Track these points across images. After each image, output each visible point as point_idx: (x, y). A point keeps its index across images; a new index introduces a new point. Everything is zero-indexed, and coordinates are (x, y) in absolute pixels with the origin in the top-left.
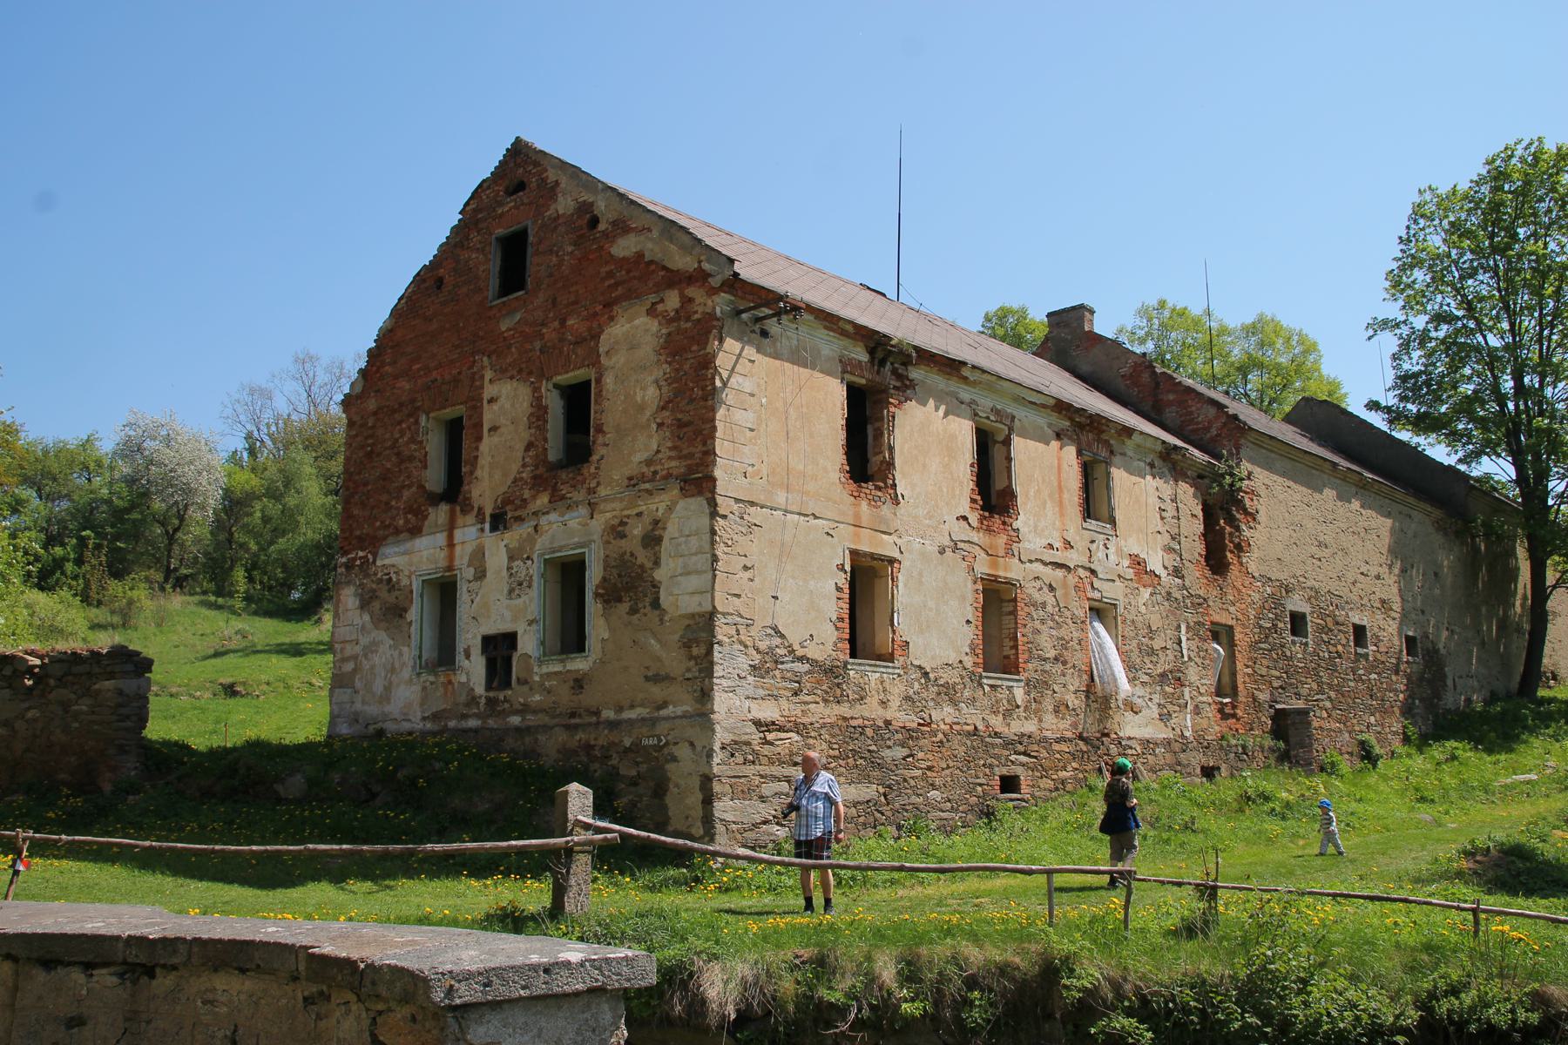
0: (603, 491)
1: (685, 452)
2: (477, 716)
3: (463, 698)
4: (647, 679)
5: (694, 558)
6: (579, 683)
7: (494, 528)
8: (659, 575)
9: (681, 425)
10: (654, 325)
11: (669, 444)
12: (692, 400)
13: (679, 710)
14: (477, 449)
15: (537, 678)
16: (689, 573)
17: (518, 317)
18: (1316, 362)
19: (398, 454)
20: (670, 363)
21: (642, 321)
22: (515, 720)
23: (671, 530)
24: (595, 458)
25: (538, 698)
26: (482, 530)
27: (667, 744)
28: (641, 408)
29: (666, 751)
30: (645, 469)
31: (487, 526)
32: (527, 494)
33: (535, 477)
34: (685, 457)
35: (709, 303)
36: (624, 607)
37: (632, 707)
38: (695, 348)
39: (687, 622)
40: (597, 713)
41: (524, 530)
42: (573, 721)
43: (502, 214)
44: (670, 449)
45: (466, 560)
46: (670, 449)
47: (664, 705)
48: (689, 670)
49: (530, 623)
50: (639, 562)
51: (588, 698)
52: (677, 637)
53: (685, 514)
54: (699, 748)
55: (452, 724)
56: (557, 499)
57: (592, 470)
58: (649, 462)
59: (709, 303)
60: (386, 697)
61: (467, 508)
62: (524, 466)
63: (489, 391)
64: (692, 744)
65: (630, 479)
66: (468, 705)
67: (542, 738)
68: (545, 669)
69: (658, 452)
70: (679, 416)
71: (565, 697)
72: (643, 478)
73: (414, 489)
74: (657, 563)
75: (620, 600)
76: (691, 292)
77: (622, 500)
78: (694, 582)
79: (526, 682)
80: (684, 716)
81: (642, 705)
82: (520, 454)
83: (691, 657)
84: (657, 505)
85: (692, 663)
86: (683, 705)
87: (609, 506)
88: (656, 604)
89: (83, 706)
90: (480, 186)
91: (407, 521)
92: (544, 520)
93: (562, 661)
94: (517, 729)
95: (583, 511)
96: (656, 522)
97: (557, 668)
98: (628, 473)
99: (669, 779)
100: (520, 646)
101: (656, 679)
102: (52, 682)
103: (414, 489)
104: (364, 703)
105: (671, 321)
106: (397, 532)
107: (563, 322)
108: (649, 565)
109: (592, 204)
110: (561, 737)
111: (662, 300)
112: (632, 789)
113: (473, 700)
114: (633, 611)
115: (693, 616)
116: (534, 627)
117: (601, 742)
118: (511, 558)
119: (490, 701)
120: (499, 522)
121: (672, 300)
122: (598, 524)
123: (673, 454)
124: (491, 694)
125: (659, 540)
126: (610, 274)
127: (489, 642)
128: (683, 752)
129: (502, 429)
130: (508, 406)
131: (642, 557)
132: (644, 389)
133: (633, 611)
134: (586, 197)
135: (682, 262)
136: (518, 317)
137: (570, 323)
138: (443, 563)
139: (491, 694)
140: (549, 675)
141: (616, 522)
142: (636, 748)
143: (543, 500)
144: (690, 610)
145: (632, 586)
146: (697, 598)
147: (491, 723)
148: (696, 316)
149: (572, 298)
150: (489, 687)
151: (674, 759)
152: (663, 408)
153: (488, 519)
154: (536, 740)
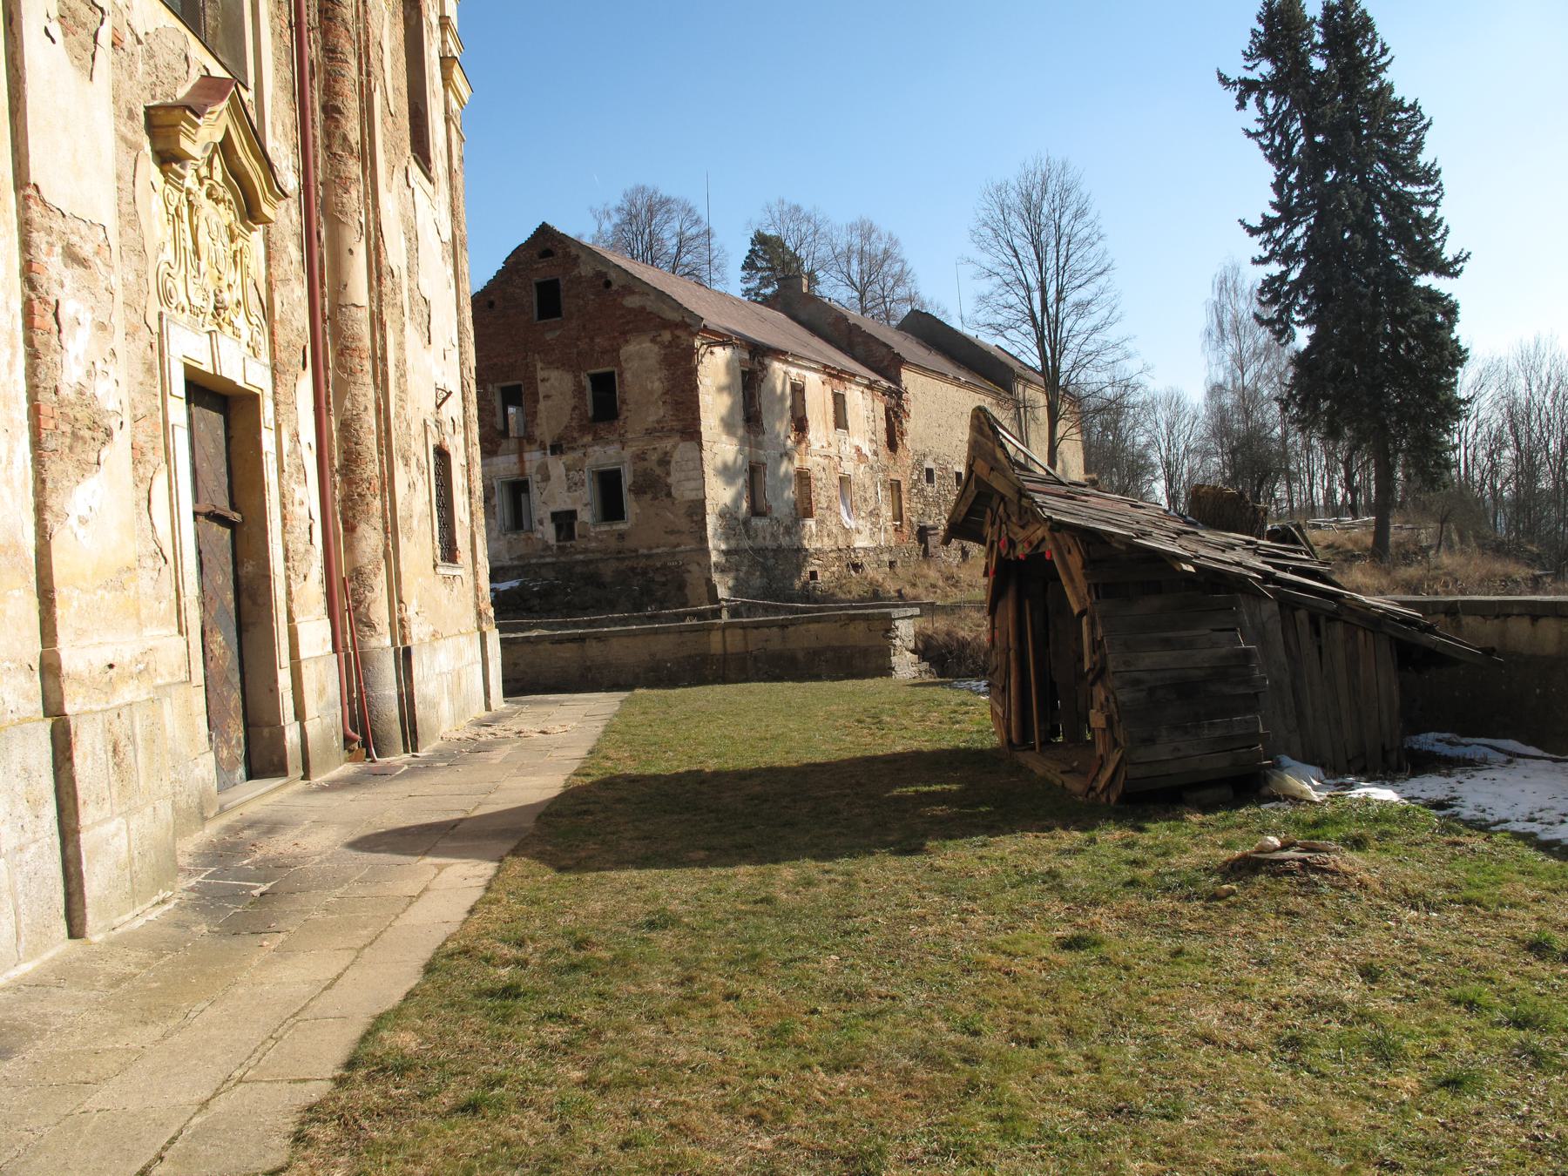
0: (629, 436)
6: (622, 536)
7: (553, 453)
8: (669, 480)
9: (677, 403)
10: (656, 348)
22: (581, 557)
23: (676, 456)
28: (651, 393)
32: (576, 435)
36: (649, 496)
41: (578, 454)
47: (678, 545)
51: (629, 543)
53: (682, 451)
56: (597, 439)
58: (658, 422)
63: (540, 374)
71: (613, 544)
72: (655, 430)
74: (668, 474)
76: (678, 332)
78: (692, 484)
84: (667, 444)
88: (669, 495)
92: (590, 450)
95: (617, 446)
96: (666, 453)
97: (606, 528)
101: (672, 532)
107: (592, 339)
113: (547, 547)
114: (655, 498)
118: (568, 470)
120: (556, 449)
121: (667, 336)
122: (627, 453)
126: (622, 316)
127: (555, 516)
128: (694, 568)
131: (658, 471)
133: (655, 498)
134: (600, 268)
142: (664, 566)
143: (588, 439)
145: (653, 485)
147: (562, 559)
150: (558, 540)
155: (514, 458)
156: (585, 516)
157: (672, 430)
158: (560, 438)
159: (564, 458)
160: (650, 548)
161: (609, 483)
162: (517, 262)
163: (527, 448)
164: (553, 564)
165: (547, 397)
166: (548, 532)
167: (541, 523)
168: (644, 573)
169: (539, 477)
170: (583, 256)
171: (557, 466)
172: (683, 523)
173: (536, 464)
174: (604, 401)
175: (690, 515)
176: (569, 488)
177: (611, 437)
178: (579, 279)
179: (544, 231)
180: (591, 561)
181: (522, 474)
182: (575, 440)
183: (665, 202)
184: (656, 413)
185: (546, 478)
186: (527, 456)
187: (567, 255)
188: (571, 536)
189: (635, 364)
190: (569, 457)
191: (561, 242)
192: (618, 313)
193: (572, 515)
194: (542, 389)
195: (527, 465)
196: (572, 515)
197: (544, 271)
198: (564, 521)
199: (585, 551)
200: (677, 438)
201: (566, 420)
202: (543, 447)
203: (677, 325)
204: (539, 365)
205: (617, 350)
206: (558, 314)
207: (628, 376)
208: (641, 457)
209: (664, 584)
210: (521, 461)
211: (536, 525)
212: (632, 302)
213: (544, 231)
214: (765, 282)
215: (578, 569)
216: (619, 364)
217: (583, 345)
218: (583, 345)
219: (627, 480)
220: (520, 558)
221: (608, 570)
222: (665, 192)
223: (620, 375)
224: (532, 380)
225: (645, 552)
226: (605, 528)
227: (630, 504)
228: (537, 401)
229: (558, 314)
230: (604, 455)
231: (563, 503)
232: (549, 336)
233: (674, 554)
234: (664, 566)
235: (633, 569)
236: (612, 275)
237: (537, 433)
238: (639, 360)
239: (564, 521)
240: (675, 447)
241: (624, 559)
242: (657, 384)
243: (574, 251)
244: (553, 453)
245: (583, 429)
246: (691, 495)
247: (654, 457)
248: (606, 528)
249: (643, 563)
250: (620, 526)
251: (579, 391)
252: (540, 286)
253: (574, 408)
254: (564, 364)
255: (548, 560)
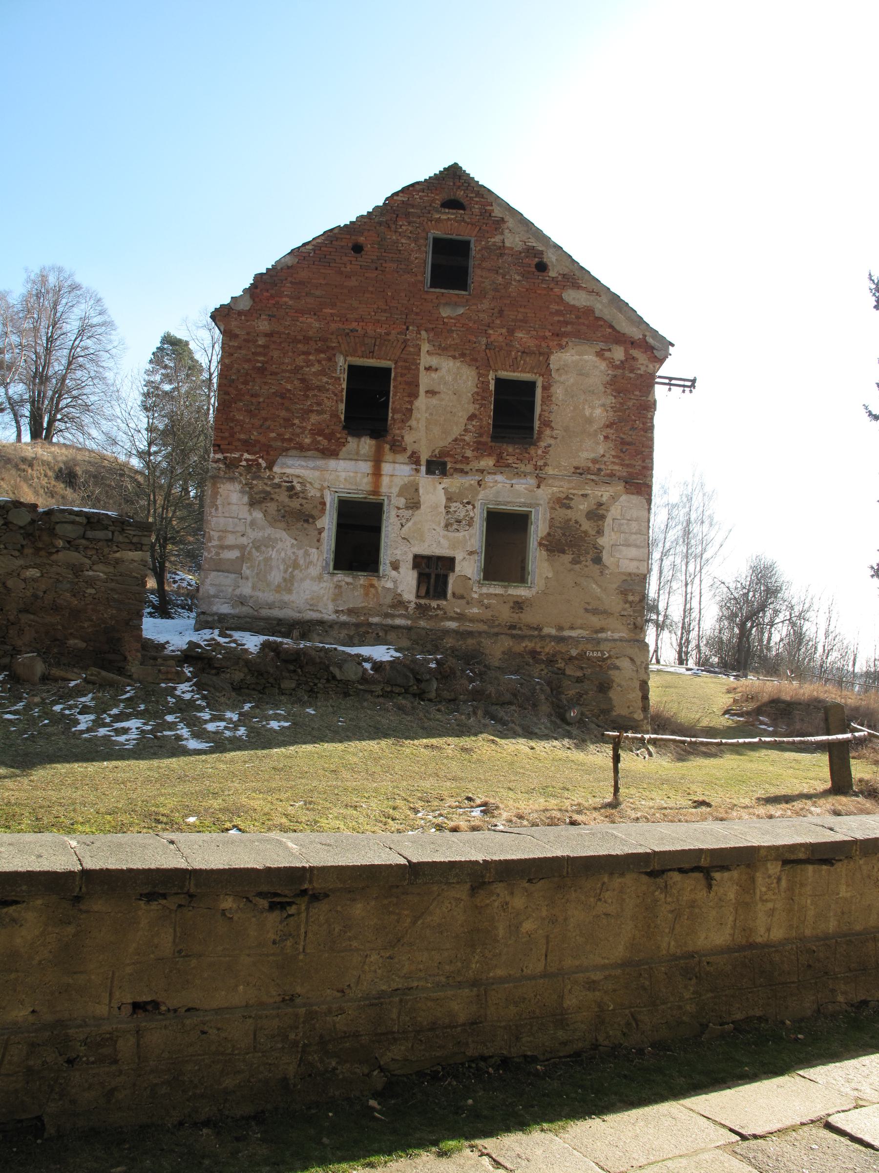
0: (550, 471)
1: (627, 462)
2: (406, 617)
3: (388, 600)
4: (586, 610)
5: (634, 537)
6: (519, 605)
7: (429, 471)
8: (601, 541)
9: (623, 443)
10: (603, 366)
11: (613, 453)
12: (633, 428)
13: (616, 636)
14: (411, 403)
15: (476, 596)
16: (628, 546)
17: (461, 311)
18: (153, 372)
19: (303, 380)
20: (615, 397)
21: (590, 358)
22: (453, 625)
23: (614, 512)
24: (542, 444)
25: (475, 610)
26: (417, 471)
27: (610, 657)
28: (590, 421)
29: (609, 662)
30: (590, 465)
31: (423, 469)
32: (469, 453)
33: (478, 443)
34: (628, 466)
35: (651, 366)
36: (567, 558)
37: (572, 628)
38: (637, 393)
39: (625, 578)
40: (539, 629)
41: (469, 481)
42: (514, 632)
43: (439, 220)
44: (614, 456)
45: (395, 490)
46: (614, 456)
47: (602, 630)
48: (625, 610)
49: (471, 553)
50: (583, 528)
51: (528, 617)
52: (615, 586)
53: (623, 505)
54: (638, 663)
55: (375, 620)
56: (501, 465)
57: (540, 452)
58: (594, 461)
59: (651, 366)
60: (288, 584)
61: (397, 447)
62: (466, 430)
63: (425, 360)
64: (632, 659)
65: (577, 468)
66: (393, 606)
67: (486, 642)
68: (485, 590)
69: (603, 456)
70: (622, 436)
71: (506, 614)
72: (588, 471)
73: (326, 416)
74: (600, 532)
75: (563, 552)
76: (635, 353)
77: (569, 482)
78: (633, 552)
79: (462, 597)
80: (621, 640)
81: (581, 628)
82: (463, 420)
83: (626, 602)
84: (604, 493)
85: (628, 605)
86: (619, 632)
87: (557, 483)
88: (598, 560)
89: (100, 572)
90: (412, 185)
91: (315, 442)
92: (489, 479)
93: (505, 587)
94: (456, 632)
95: (532, 481)
96: (600, 505)
97: (499, 591)
98: (575, 464)
99: (613, 681)
100: (457, 568)
101: (595, 612)
102: (60, 543)
103: (326, 416)
104: (254, 588)
105: (616, 367)
106: (301, 448)
107: (511, 332)
108: (592, 532)
109: (542, 253)
110: (506, 643)
111: (610, 350)
112: (578, 685)
113: (399, 603)
114: (575, 562)
115: (630, 574)
116: (476, 557)
117: (547, 650)
118: (449, 499)
119: (419, 606)
120: (437, 466)
121: (618, 353)
122: (544, 494)
123: (616, 460)
124: (423, 601)
125: (603, 517)
126: (558, 313)
127: (421, 562)
128: (625, 663)
129: (442, 396)
130: (449, 378)
131: (586, 525)
132: (593, 408)
133: (575, 562)
134: (533, 243)
135: (635, 333)
136: (461, 311)
137: (519, 334)
138: (369, 488)
139: (423, 601)
140: (489, 596)
141: (563, 496)
142: (582, 656)
143: (488, 462)
144: (629, 570)
145: (574, 542)
146: (635, 563)
147: (422, 623)
148: (639, 372)
149: (520, 317)
150: (418, 596)
151: (617, 668)
152: (607, 426)
153: (423, 462)
154: (479, 643)
155: (366, 467)
156: (468, 567)
157: (612, 475)
158: (444, 453)
159: (447, 482)
160: (561, 628)
161: (505, 532)
162: (403, 205)
163: (389, 456)
164: (409, 629)
165: (431, 393)
166: (406, 582)
167: (395, 566)
168: (551, 661)
169: (402, 502)
170: (511, 223)
171: (434, 492)
172: (613, 602)
173: (399, 482)
174: (513, 416)
175: (624, 593)
176: (447, 526)
177: (522, 467)
178: (501, 250)
179: (454, 173)
180: (470, 634)
181: (376, 492)
182: (466, 460)
183: (75, 287)
184: (593, 448)
185: (414, 505)
186: (386, 468)
187: (486, 214)
188: (441, 593)
189: (570, 379)
190: (455, 483)
191: (478, 194)
192: (554, 307)
193: (449, 563)
194: (425, 381)
195: (385, 480)
196: (449, 563)
197: (447, 224)
198: (434, 572)
199: (460, 617)
200: (620, 487)
201: (456, 431)
202: (414, 459)
203: (633, 343)
204: (425, 347)
205: (547, 355)
206: (464, 286)
207: (558, 392)
208: (563, 502)
209: (579, 680)
210: (377, 473)
211: (385, 567)
212: (574, 297)
213: (454, 173)
214: (167, 378)
215: (449, 642)
216: (546, 372)
217: (497, 335)
218: (497, 335)
219: (539, 529)
220: (350, 612)
221: (496, 650)
222: (79, 279)
223: (545, 388)
224: (411, 367)
225: (553, 632)
226: (496, 589)
227: (539, 564)
228: (415, 395)
229: (464, 286)
230: (507, 489)
231: (436, 543)
232: (445, 312)
233: (599, 642)
234: (582, 656)
235: (534, 654)
236: (550, 257)
237: (409, 439)
238: (575, 380)
239: (434, 572)
240: (614, 498)
241: (522, 638)
242: (598, 412)
243: (497, 212)
244: (429, 471)
245: (480, 448)
246: (631, 567)
247: (584, 506)
248: (499, 591)
249: (550, 647)
250: (521, 592)
251: (479, 396)
252: (438, 244)
253: (472, 417)
254: (464, 354)
255: (398, 622)
